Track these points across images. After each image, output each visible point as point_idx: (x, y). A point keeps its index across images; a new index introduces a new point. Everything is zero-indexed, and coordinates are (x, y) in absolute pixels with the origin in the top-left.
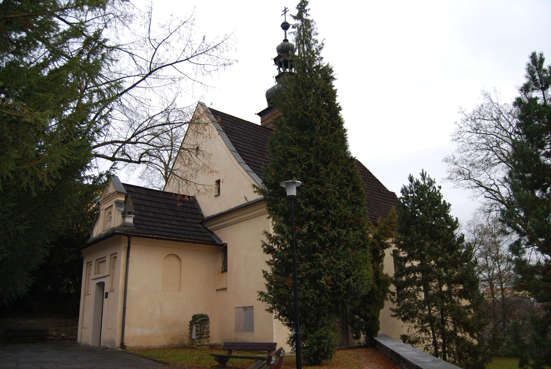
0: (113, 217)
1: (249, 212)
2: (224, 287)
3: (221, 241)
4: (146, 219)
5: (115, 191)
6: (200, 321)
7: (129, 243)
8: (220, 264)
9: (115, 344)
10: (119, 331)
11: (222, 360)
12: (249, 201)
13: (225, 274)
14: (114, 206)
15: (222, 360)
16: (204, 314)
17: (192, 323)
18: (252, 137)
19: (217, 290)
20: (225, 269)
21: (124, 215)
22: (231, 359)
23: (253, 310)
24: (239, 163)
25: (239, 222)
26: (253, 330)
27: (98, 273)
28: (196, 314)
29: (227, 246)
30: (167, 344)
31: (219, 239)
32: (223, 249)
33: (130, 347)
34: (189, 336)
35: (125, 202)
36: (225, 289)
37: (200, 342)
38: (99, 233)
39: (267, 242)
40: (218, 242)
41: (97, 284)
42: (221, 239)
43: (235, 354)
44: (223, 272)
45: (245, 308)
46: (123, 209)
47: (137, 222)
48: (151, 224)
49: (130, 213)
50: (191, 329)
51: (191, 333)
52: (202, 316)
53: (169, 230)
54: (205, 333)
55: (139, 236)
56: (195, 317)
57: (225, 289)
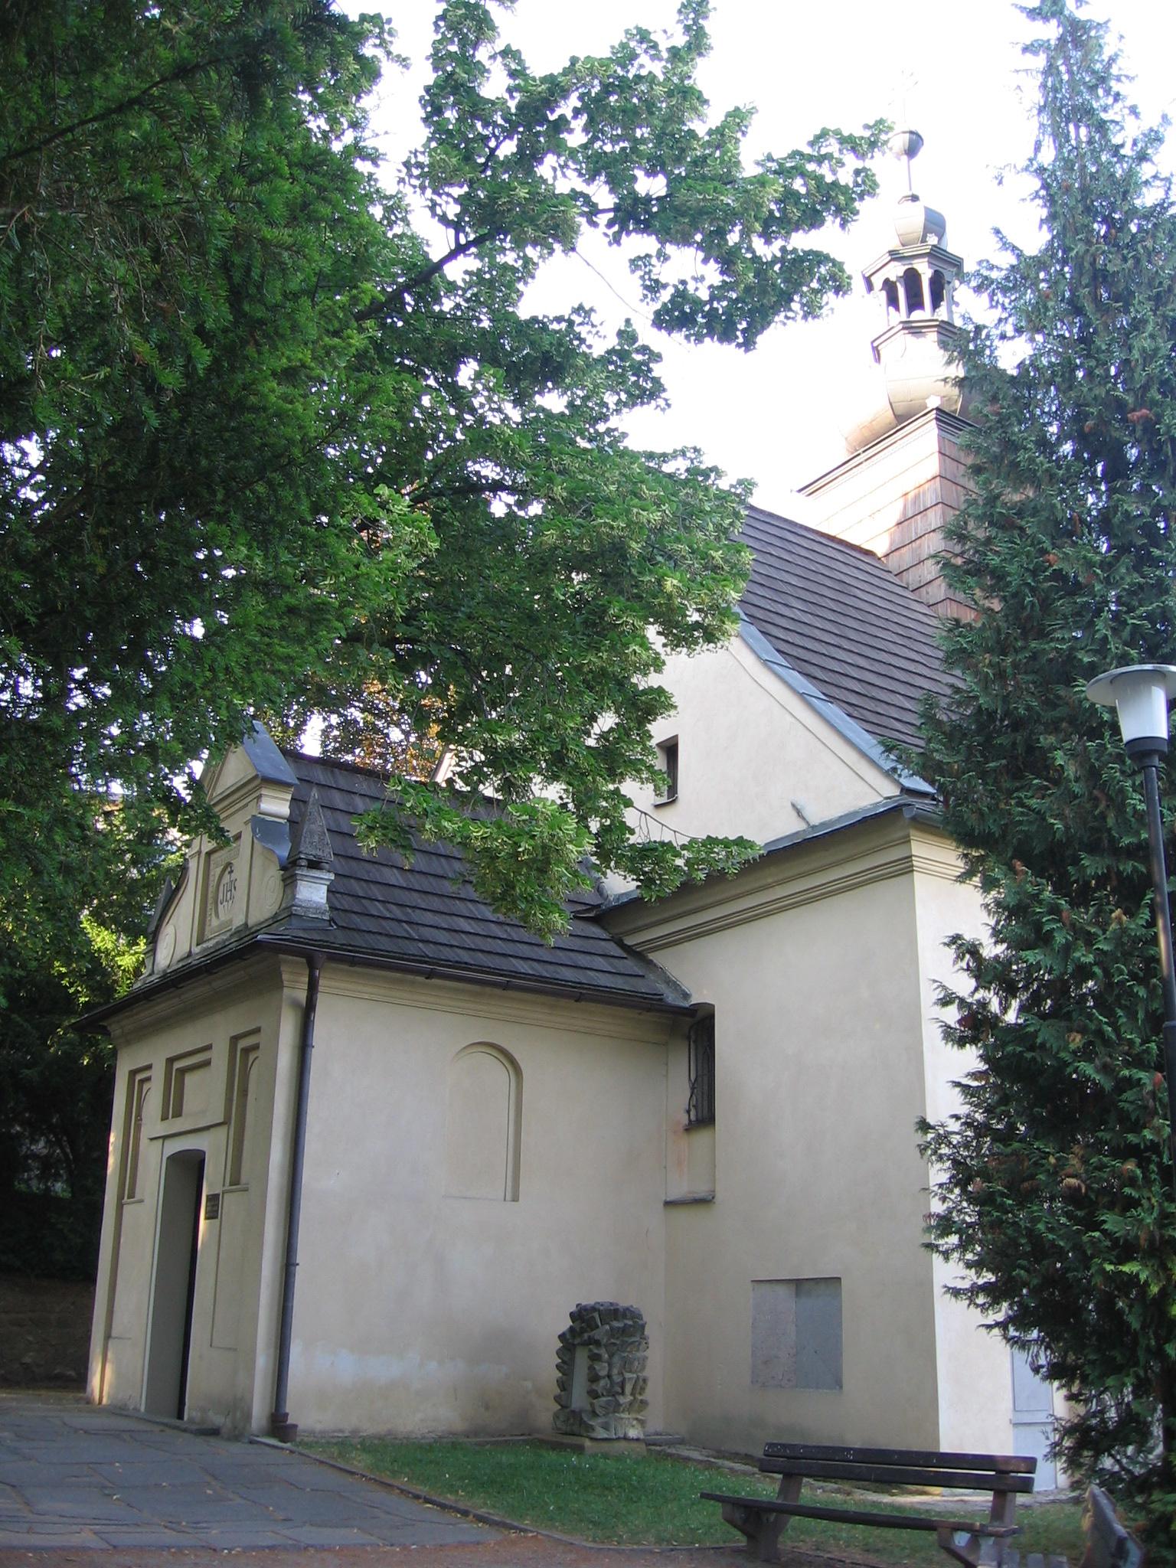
0: (241, 885)
1: (720, 903)
2: (701, 1190)
3: (686, 996)
4: (376, 892)
5: (252, 773)
6: (599, 1336)
7: (313, 988)
8: (676, 1090)
9: (248, 1416)
10: (263, 1361)
11: (754, 1520)
12: (815, 821)
13: (701, 1137)
14: (247, 837)
15: (754, 1520)
16: (623, 1303)
17: (570, 1342)
18: (799, 571)
19: (668, 1204)
20: (703, 1114)
21: (290, 872)
22: (795, 1520)
23: (838, 1295)
24: (766, 663)
25: (690, 939)
26: (838, 1383)
27: (178, 1113)
28: (588, 1301)
29: (711, 1017)
30: (459, 1426)
31: (674, 985)
32: (694, 1029)
33: (312, 1433)
34: (557, 1399)
35: (294, 822)
36: (704, 1202)
37: (606, 1427)
38: (183, 949)
39: (964, 985)
40: (671, 998)
41: (173, 1159)
42: (687, 985)
43: (815, 1492)
44: (692, 1127)
45: (798, 1285)
46: (284, 851)
47: (346, 903)
48: (397, 912)
49: (315, 865)
50: (566, 1366)
51: (564, 1385)
52: (613, 1313)
53: (469, 941)
54: (628, 1388)
55: (353, 962)
56: (584, 1318)
57: (704, 1202)
